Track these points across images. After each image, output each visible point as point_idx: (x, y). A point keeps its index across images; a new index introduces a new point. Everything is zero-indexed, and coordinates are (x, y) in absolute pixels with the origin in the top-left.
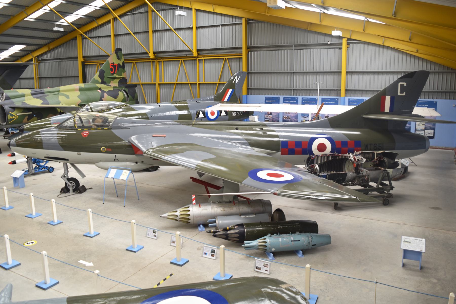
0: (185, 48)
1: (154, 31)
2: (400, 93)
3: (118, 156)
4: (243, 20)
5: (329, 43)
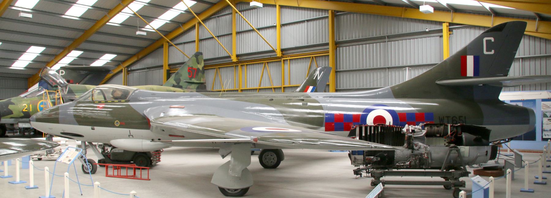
0: (269, 48)
1: (238, 33)
2: (487, 51)
3: (133, 131)
4: (330, 12)
5: (427, 30)
